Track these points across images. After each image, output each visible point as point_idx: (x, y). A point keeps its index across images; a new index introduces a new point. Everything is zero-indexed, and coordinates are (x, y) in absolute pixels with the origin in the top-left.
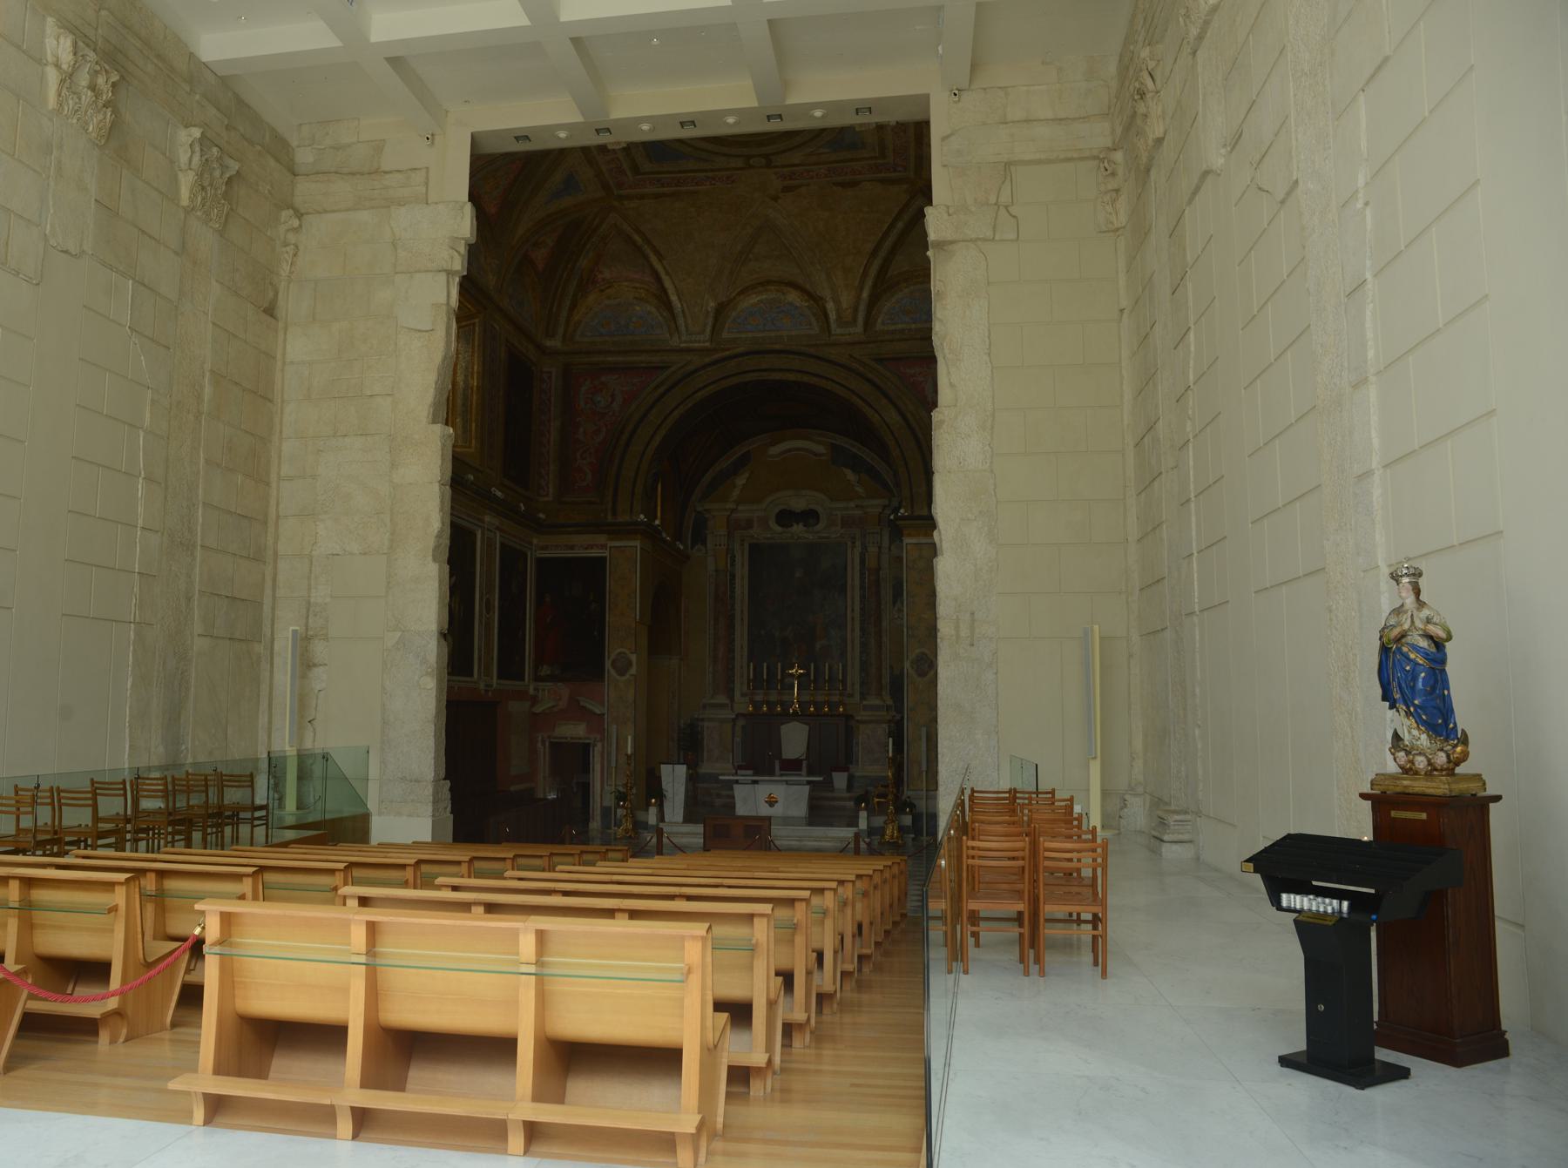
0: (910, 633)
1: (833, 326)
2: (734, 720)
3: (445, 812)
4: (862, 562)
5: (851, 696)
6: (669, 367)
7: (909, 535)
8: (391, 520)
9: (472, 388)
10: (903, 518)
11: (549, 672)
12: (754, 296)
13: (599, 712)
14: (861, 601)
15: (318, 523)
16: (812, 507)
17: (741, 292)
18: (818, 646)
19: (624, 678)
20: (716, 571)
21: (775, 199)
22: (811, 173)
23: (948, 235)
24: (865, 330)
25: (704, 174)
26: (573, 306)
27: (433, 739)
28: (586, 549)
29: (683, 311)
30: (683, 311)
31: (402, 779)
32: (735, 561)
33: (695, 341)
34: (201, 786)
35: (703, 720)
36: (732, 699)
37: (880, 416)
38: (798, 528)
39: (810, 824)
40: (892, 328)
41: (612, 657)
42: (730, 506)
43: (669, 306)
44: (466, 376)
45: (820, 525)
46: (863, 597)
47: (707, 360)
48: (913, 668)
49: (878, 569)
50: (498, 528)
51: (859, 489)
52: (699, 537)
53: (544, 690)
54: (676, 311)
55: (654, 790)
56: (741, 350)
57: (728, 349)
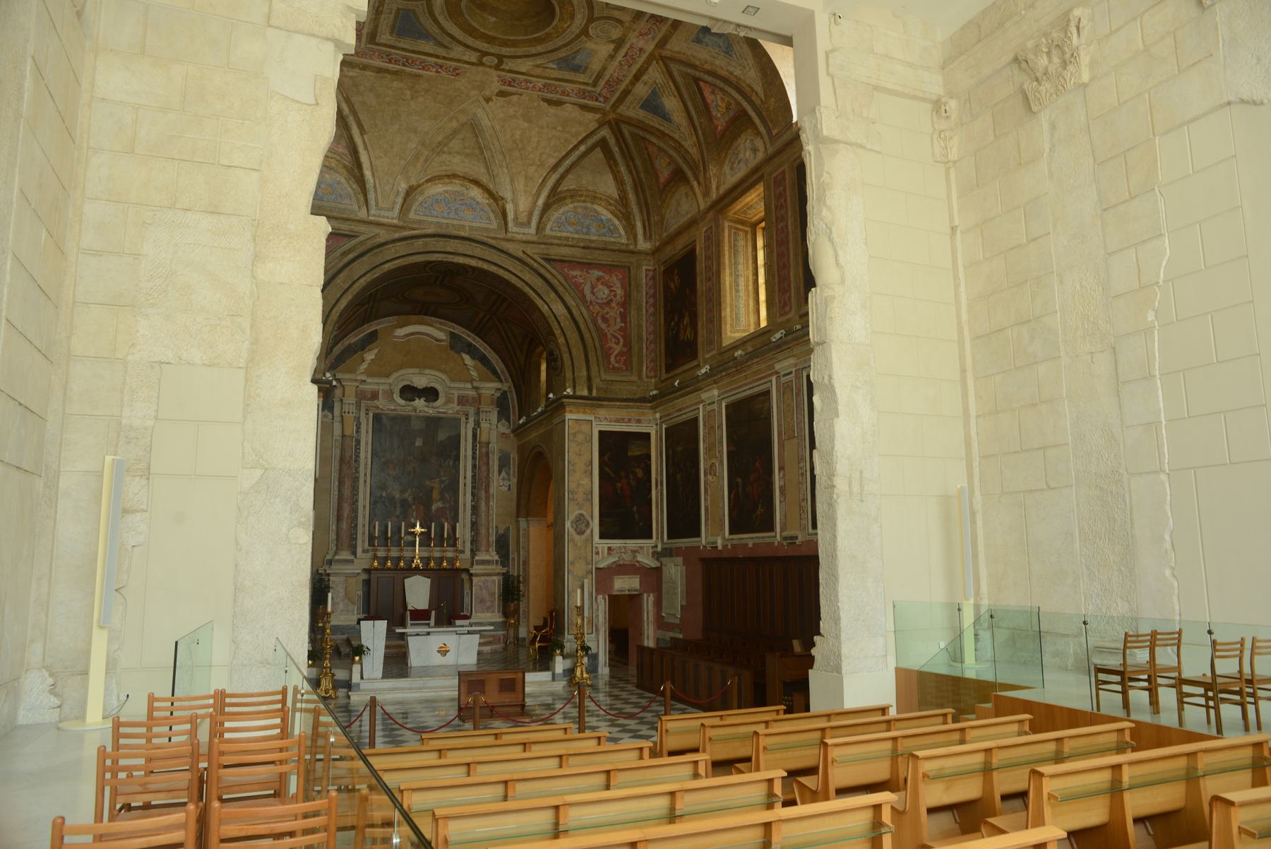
0: (571, 496)
1: (510, 225)
4: (474, 435)
5: (462, 552)
6: (357, 237)
7: (571, 412)
8: (252, 326)
10: (568, 397)
12: (440, 186)
14: (472, 469)
15: (139, 318)
16: (433, 385)
18: (434, 507)
21: (488, 100)
22: (528, 84)
23: (836, 134)
24: (537, 233)
25: (435, 60)
29: (375, 187)
30: (375, 187)
32: (359, 428)
33: (384, 217)
34: (1260, 647)
36: (354, 554)
37: (548, 306)
38: (420, 403)
40: (559, 234)
43: (361, 182)
45: (439, 401)
46: (474, 466)
47: (397, 236)
48: (572, 527)
49: (488, 443)
51: (474, 373)
54: (367, 186)
56: (430, 231)
57: (414, 229)
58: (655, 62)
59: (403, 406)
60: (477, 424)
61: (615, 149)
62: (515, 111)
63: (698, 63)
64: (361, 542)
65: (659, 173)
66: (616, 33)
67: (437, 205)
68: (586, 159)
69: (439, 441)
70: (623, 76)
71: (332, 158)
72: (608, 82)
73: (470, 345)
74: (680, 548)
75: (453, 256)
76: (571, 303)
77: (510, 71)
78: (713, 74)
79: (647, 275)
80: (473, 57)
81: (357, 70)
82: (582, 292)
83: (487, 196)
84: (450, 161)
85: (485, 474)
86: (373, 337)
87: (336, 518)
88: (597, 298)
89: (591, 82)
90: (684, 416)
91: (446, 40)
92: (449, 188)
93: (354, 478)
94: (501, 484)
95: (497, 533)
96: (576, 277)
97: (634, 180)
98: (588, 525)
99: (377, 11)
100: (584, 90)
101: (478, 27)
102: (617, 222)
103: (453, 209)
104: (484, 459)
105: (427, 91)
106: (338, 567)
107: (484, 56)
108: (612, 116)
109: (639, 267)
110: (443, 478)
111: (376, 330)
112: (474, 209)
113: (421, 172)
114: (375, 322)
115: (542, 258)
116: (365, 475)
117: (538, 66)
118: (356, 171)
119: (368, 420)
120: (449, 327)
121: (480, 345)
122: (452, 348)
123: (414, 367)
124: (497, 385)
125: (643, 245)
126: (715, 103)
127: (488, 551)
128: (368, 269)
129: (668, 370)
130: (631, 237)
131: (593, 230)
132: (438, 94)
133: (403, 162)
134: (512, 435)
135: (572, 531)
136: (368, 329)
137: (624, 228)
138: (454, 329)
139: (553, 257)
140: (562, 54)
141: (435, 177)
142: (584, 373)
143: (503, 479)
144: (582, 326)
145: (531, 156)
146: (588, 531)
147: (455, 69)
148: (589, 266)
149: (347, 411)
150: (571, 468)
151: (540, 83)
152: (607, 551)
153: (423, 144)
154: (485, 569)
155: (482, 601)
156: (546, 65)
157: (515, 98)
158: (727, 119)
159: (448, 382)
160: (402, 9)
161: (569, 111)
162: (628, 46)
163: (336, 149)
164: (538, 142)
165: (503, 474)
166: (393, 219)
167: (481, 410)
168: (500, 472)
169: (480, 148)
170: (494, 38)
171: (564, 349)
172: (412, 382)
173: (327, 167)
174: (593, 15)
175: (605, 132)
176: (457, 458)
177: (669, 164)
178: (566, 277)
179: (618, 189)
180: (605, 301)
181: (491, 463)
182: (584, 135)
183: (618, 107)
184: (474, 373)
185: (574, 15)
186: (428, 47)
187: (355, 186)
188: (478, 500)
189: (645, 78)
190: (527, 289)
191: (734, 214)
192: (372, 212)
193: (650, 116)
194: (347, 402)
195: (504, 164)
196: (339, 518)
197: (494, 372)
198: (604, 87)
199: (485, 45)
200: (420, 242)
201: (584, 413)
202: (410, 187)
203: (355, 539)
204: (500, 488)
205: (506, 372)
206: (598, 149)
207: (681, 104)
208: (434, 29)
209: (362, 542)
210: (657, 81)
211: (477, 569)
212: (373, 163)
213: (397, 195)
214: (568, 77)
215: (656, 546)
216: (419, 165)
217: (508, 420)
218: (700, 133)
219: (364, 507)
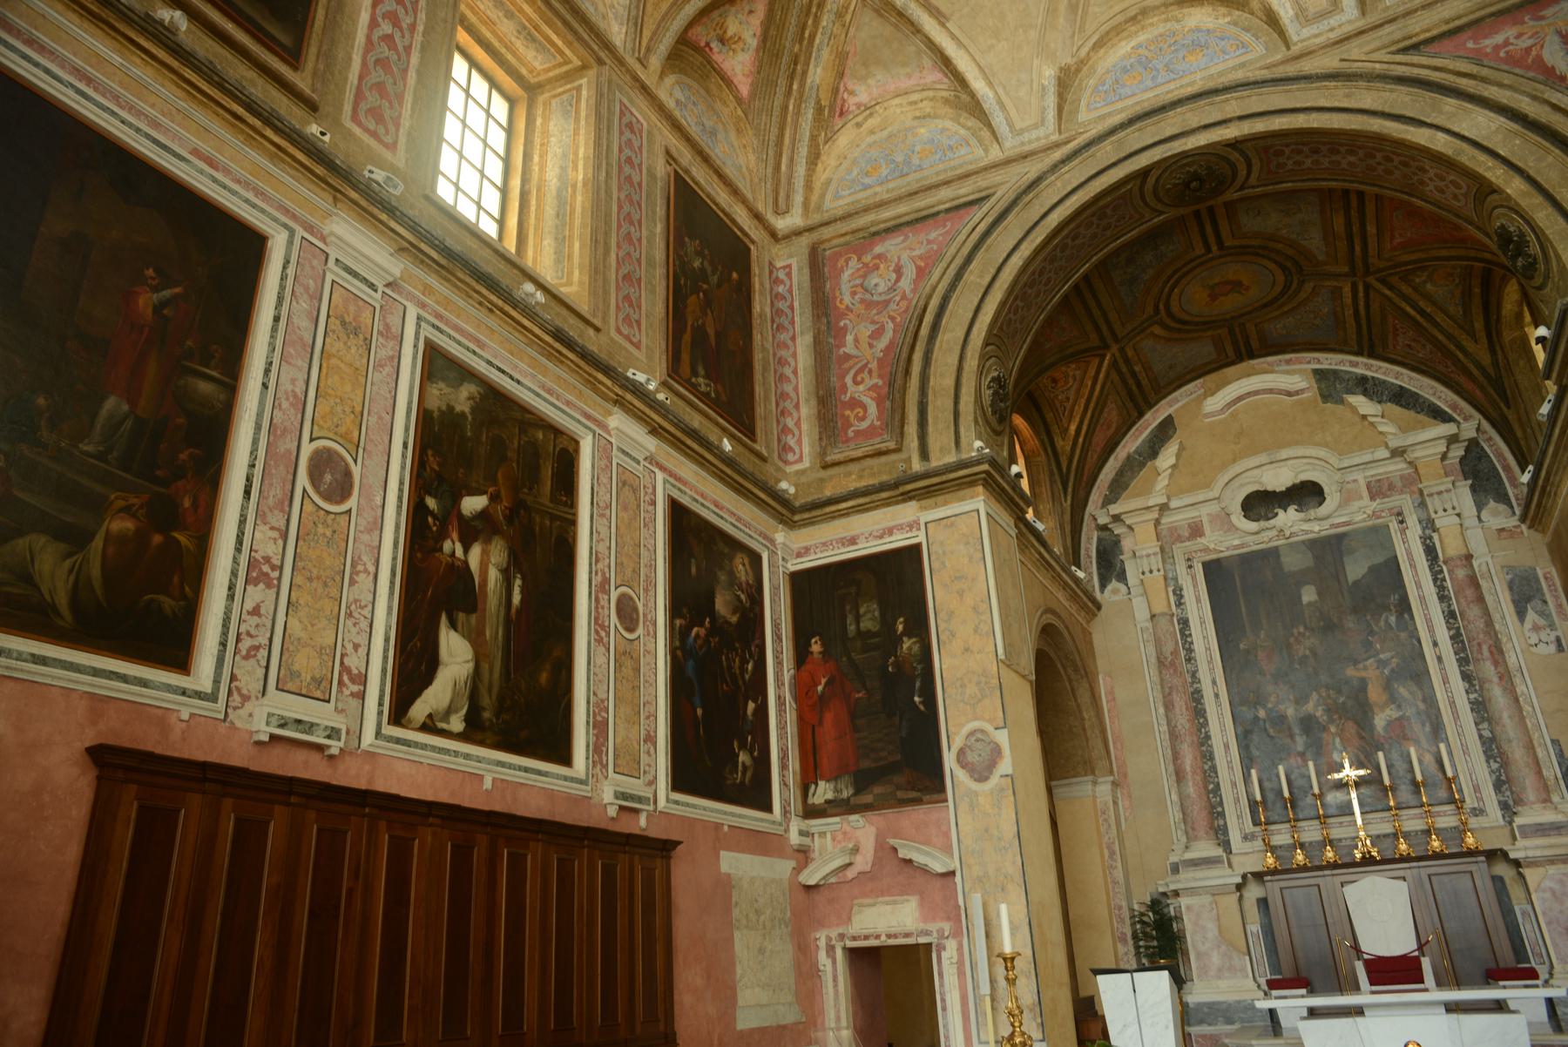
2: (1239, 887)
4: (1430, 551)
5: (1478, 812)
9: (574, 186)
11: (830, 796)
12: (1123, 43)
13: (939, 868)
17: (1098, 45)
20: (1153, 616)
26: (814, 158)
28: (881, 537)
35: (1176, 894)
36: (1226, 846)
38: (1288, 518)
41: (955, 749)
42: (1157, 499)
43: (975, 108)
44: (563, 169)
46: (1450, 616)
49: (1469, 557)
52: (1110, 563)
53: (822, 835)
54: (985, 106)
59: (1257, 533)
60: (1429, 524)
64: (1234, 818)
67: (1126, 77)
69: (1350, 583)
71: (922, 101)
75: (1184, 140)
85: (1481, 624)
86: (1166, 429)
87: (1174, 778)
92: (1142, 37)
93: (1193, 693)
94: (1534, 640)
96: (1507, 43)
103: (1160, 66)
104: (1470, 593)
106: (1191, 875)
110: (1382, 656)
111: (1170, 416)
113: (1073, 36)
114: (1163, 402)
115: (1393, 53)
116: (1214, 682)
119: (1194, 578)
120: (1309, 362)
121: (1384, 374)
122: (1326, 397)
123: (1256, 453)
127: (1547, 800)
128: (1020, 236)
133: (1033, 34)
134: (1524, 527)
136: (1154, 419)
138: (1319, 361)
139: (1422, 37)
141: (1108, 33)
143: (1536, 628)
149: (1147, 570)
154: (1551, 846)
159: (1334, 460)
163: (923, 81)
165: (1531, 616)
167: (1425, 493)
168: (1521, 614)
172: (1260, 483)
173: (918, 118)
176: (1404, 606)
178: (1477, 58)
181: (1489, 599)
187: (972, 122)
188: (1481, 686)
194: (1144, 553)
200: (1107, 145)
202: (1061, 69)
203: (1222, 815)
204: (1534, 649)
205: (1463, 404)
209: (1237, 821)
211: (1526, 849)
212: (982, 63)
213: (1043, 96)
216: (1061, 20)
217: (1503, 498)
219: (1227, 746)
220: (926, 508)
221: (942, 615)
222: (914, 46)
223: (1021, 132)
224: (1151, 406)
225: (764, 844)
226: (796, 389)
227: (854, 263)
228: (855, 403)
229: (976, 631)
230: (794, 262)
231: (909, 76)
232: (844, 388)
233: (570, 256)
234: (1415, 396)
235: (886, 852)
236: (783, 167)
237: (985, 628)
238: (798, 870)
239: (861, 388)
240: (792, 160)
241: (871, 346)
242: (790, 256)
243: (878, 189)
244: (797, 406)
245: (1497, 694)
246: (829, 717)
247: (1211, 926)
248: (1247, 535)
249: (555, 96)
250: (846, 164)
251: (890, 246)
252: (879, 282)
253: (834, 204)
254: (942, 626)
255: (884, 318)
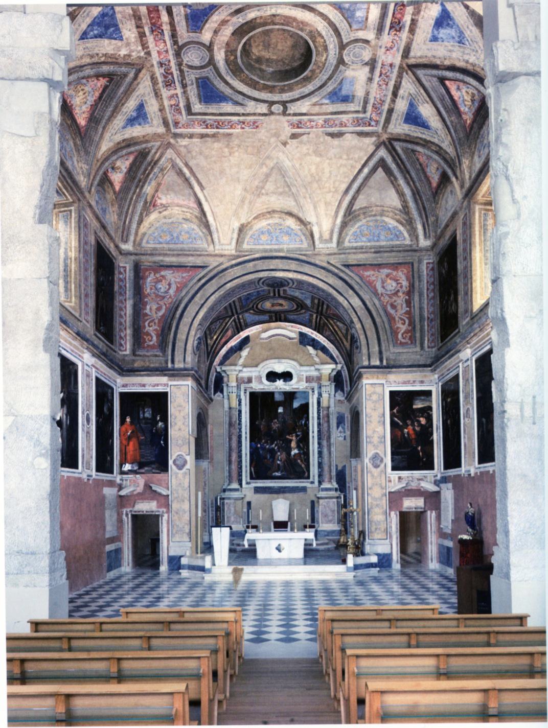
1: (317, 242)
3: (61, 579)
4: (319, 403)
7: (367, 378)
9: (71, 259)
11: (130, 468)
13: (164, 493)
17: (255, 218)
18: (293, 453)
19: (181, 472)
21: (285, 144)
23: (515, 67)
26: (140, 222)
27: (48, 515)
30: (217, 229)
31: (18, 552)
36: (241, 485)
39: (305, 564)
40: (355, 245)
41: (173, 459)
43: (207, 226)
44: (66, 249)
46: (319, 424)
49: (328, 408)
50: (94, 366)
53: (126, 480)
54: (212, 229)
55: (208, 548)
56: (257, 256)
57: (246, 256)
58: (405, 73)
60: (320, 395)
61: (393, 166)
62: (308, 149)
63: (438, 62)
65: (431, 179)
66: (367, 55)
68: (372, 180)
70: (385, 95)
72: (374, 105)
73: (314, 340)
74: (450, 476)
76: (366, 297)
77: (295, 115)
78: (452, 68)
79: (427, 268)
80: (263, 108)
81: (187, 139)
82: (375, 288)
83: (299, 223)
84: (268, 201)
88: (386, 290)
89: (360, 109)
90: (451, 374)
91: (240, 98)
92: (270, 221)
95: (337, 469)
96: (369, 276)
97: (412, 190)
98: (382, 461)
99: (183, 85)
100: (357, 118)
101: (257, 80)
102: (401, 228)
104: (326, 419)
105: (239, 146)
107: (272, 105)
108: (385, 137)
109: (420, 262)
112: (290, 235)
117: (314, 105)
118: (204, 219)
124: (333, 366)
125: (424, 243)
126: (462, 99)
129: (442, 341)
130: (414, 239)
131: (382, 237)
132: (248, 147)
133: (234, 207)
135: (370, 465)
137: (408, 231)
140: (330, 88)
142: (377, 349)
143: (340, 432)
144: (374, 314)
145: (327, 185)
146: (382, 465)
147: (254, 123)
148: (379, 266)
150: (368, 419)
151: (320, 120)
152: (398, 479)
153: (245, 190)
155: (326, 516)
156: (321, 102)
157: (305, 137)
158: (474, 110)
160: (199, 78)
161: (350, 140)
162: (379, 65)
164: (330, 172)
165: (340, 428)
166: (231, 250)
168: (338, 427)
169: (288, 186)
170: (274, 87)
171: (361, 332)
174: (342, 42)
175: (383, 153)
176: (308, 419)
177: (438, 169)
178: (361, 278)
179: (401, 200)
180: (393, 292)
182: (365, 158)
183: (387, 127)
184: (317, 360)
185: (326, 46)
186: (228, 107)
187: (204, 230)
189: (401, 92)
190: (331, 291)
191: (483, 197)
192: (217, 247)
193: (413, 128)
195: (307, 196)
196: (230, 462)
197: (332, 357)
198: (373, 111)
199: (270, 95)
200: (251, 264)
201: (378, 378)
203: (241, 476)
205: (340, 357)
206: (380, 169)
207: (434, 109)
208: (228, 91)
210: (411, 92)
214: (342, 109)
215: (436, 476)
217: (343, 390)
218: (452, 131)
219: (246, 454)
220: (171, 380)
221: (173, 417)
222: (188, 191)
223: (223, 245)
224: (242, 330)
225: (111, 484)
226: (125, 321)
227: (152, 275)
228: (148, 334)
229: (183, 424)
230: (128, 266)
231: (184, 200)
232: (145, 327)
233: (71, 290)
234: (327, 350)
235: (148, 487)
236: (127, 222)
237: (186, 424)
238: (119, 491)
239: (151, 328)
240: (131, 220)
241: (156, 313)
242: (126, 263)
243: (165, 246)
244: (125, 329)
245: (325, 451)
246: (131, 443)
247: (232, 509)
248: (266, 386)
249: (61, 212)
250: (153, 229)
251: (167, 273)
252: (163, 287)
253: (148, 245)
254: (173, 420)
255: (161, 303)
